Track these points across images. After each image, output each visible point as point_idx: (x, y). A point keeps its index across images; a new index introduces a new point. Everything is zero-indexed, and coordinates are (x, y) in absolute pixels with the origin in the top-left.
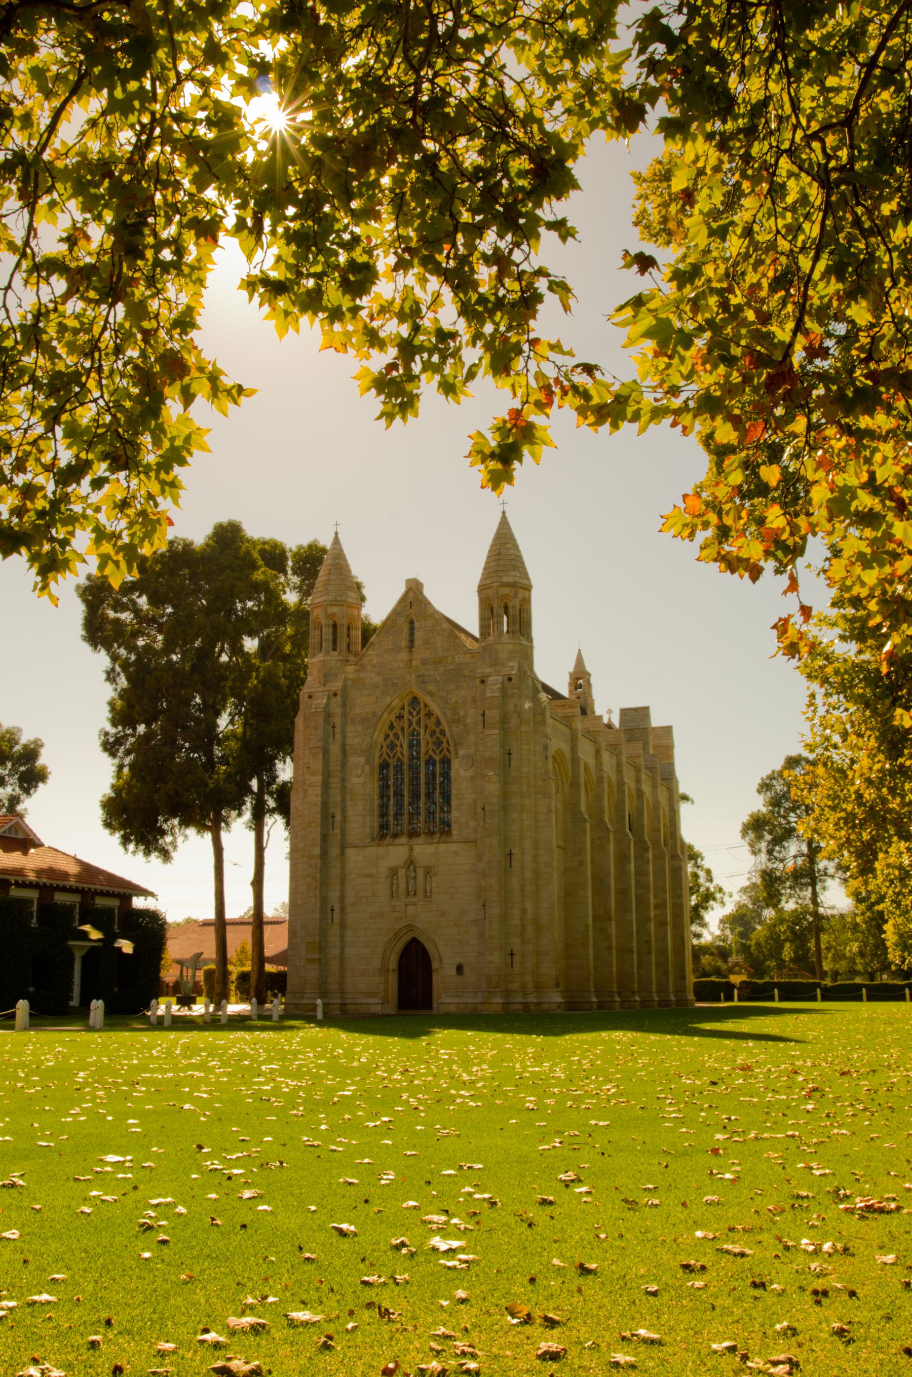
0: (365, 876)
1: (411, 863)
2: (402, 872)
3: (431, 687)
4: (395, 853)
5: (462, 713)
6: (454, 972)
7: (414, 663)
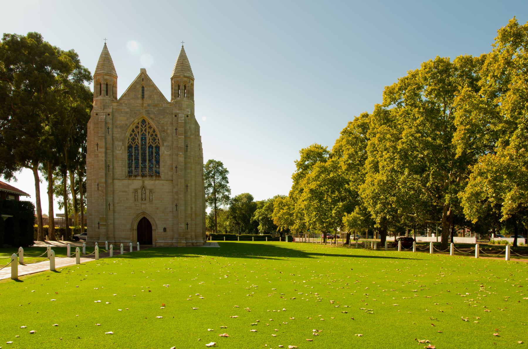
0: (123, 192)
1: (143, 187)
2: (139, 191)
3: (152, 116)
5: (165, 128)
6: (162, 231)
7: (144, 105)
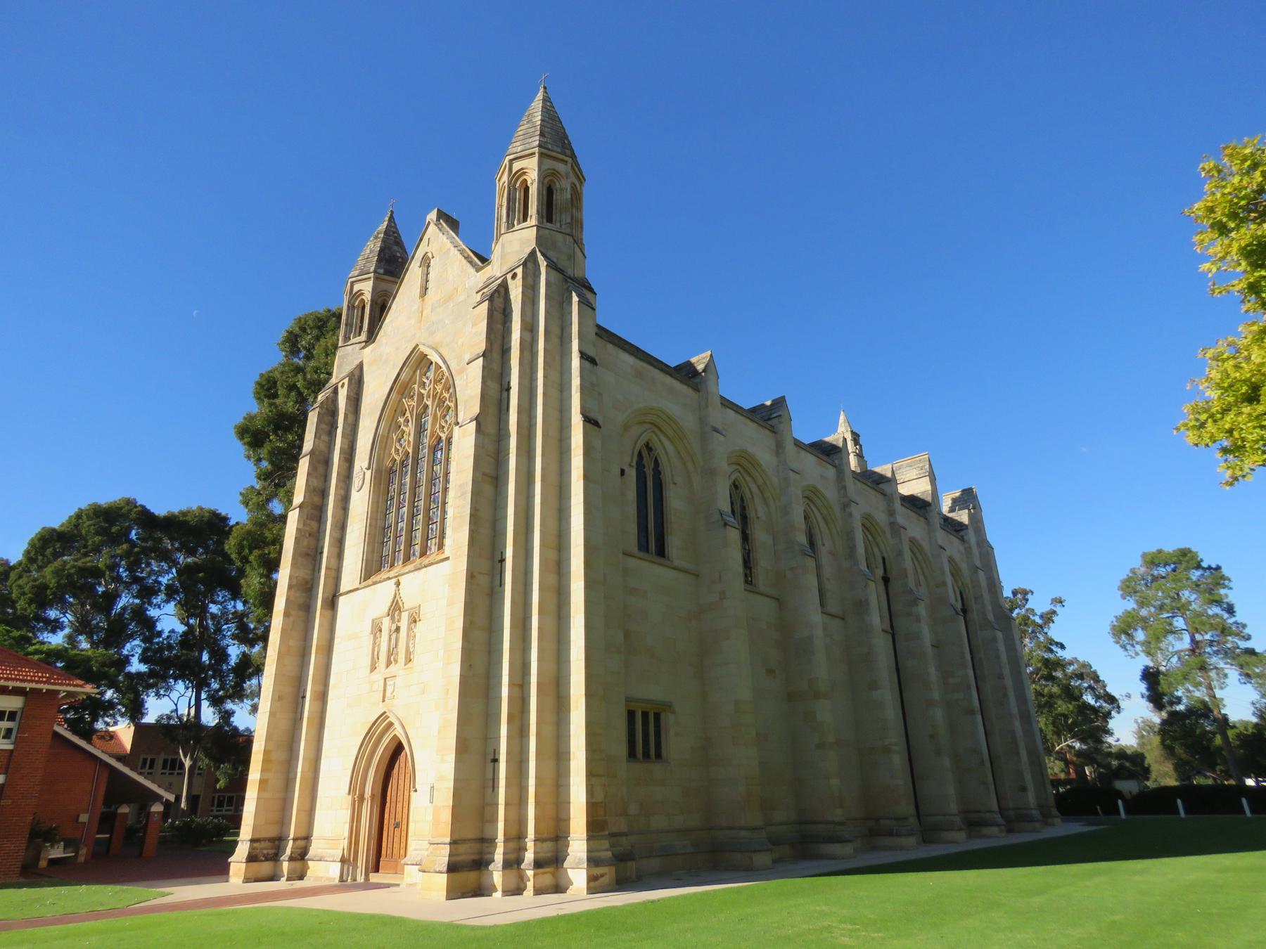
1: (395, 608)
4: (380, 594)
